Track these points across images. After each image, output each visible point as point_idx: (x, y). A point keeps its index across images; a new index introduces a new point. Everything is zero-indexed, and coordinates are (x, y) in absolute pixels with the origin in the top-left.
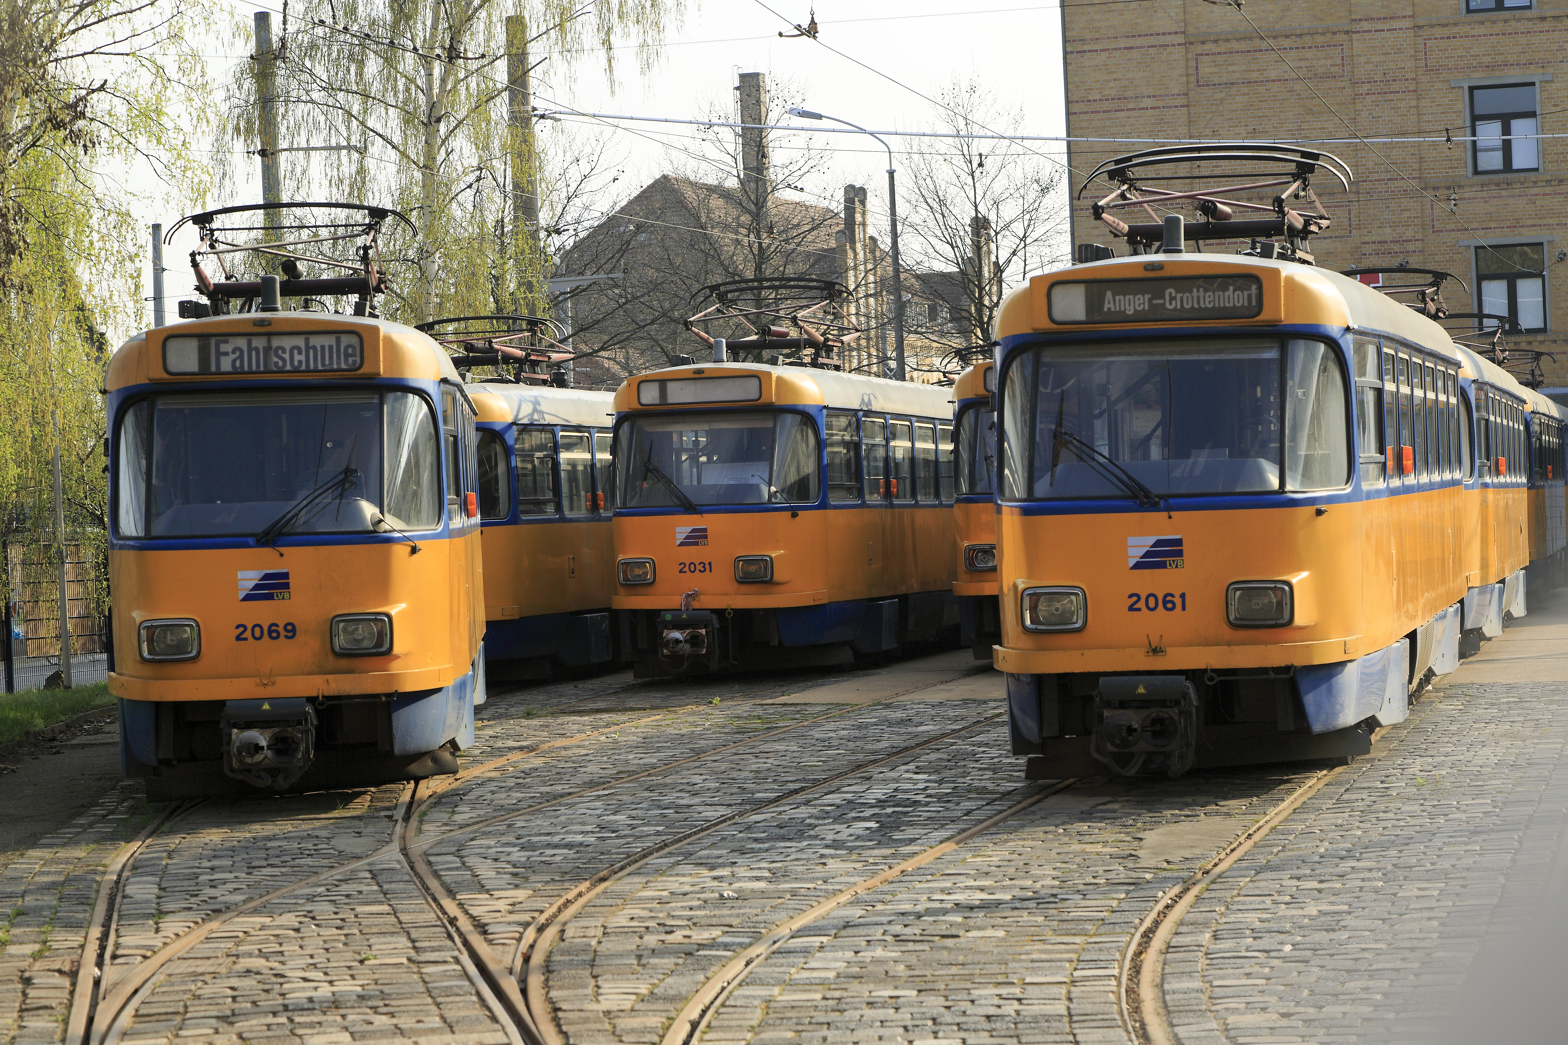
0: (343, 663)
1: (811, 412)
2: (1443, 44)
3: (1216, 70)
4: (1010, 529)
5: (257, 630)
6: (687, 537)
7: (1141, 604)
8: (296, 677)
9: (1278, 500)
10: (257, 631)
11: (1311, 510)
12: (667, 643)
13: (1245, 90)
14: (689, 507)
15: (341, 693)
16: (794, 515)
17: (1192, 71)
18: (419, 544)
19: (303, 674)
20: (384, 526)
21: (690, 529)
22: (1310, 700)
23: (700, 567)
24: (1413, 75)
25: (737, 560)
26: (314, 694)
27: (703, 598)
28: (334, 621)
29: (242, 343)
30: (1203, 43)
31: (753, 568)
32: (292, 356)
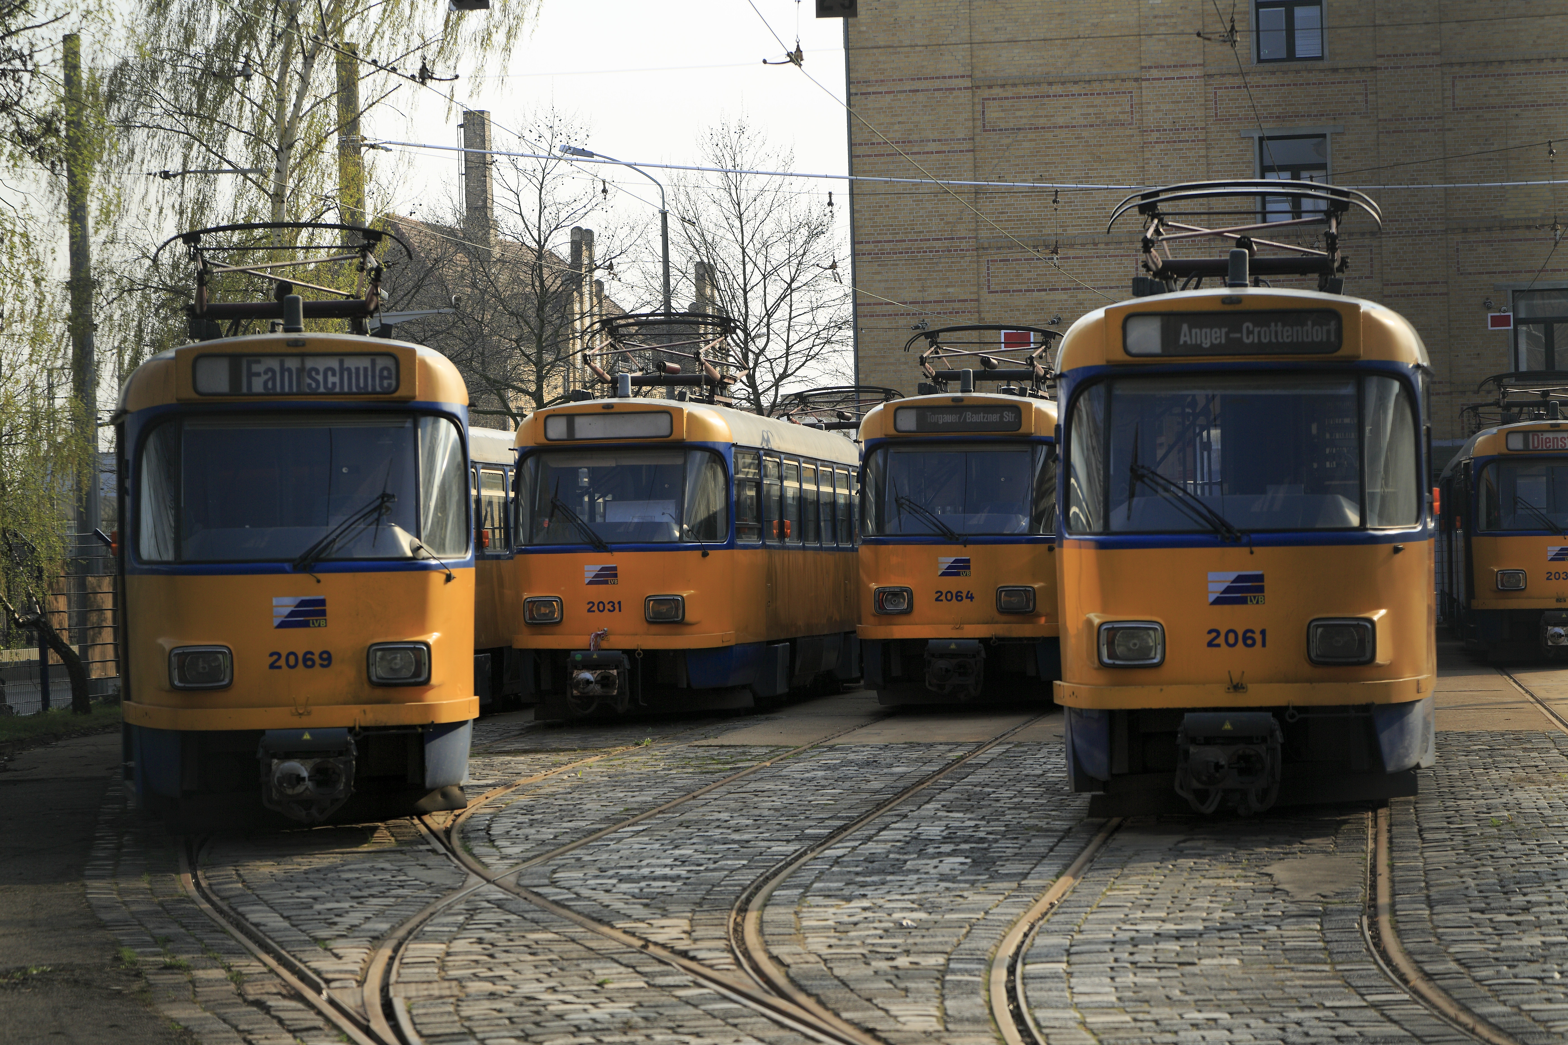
0: (379, 693)
1: (721, 449)
3: (1002, 115)
4: (1076, 562)
6: (596, 576)
7: (1221, 640)
8: (333, 707)
9: (1359, 538)
10: (292, 659)
11: (1388, 547)
12: (577, 684)
13: (1031, 135)
14: (599, 546)
15: (379, 724)
16: (705, 555)
17: (978, 115)
18: (454, 572)
19: (337, 703)
20: (423, 553)
21: (599, 567)
22: (1385, 738)
23: (609, 607)
24: (1203, 125)
25: (647, 599)
26: (351, 725)
27: (612, 638)
28: (370, 651)
29: (275, 364)
30: (990, 87)
31: (664, 608)
32: (328, 379)
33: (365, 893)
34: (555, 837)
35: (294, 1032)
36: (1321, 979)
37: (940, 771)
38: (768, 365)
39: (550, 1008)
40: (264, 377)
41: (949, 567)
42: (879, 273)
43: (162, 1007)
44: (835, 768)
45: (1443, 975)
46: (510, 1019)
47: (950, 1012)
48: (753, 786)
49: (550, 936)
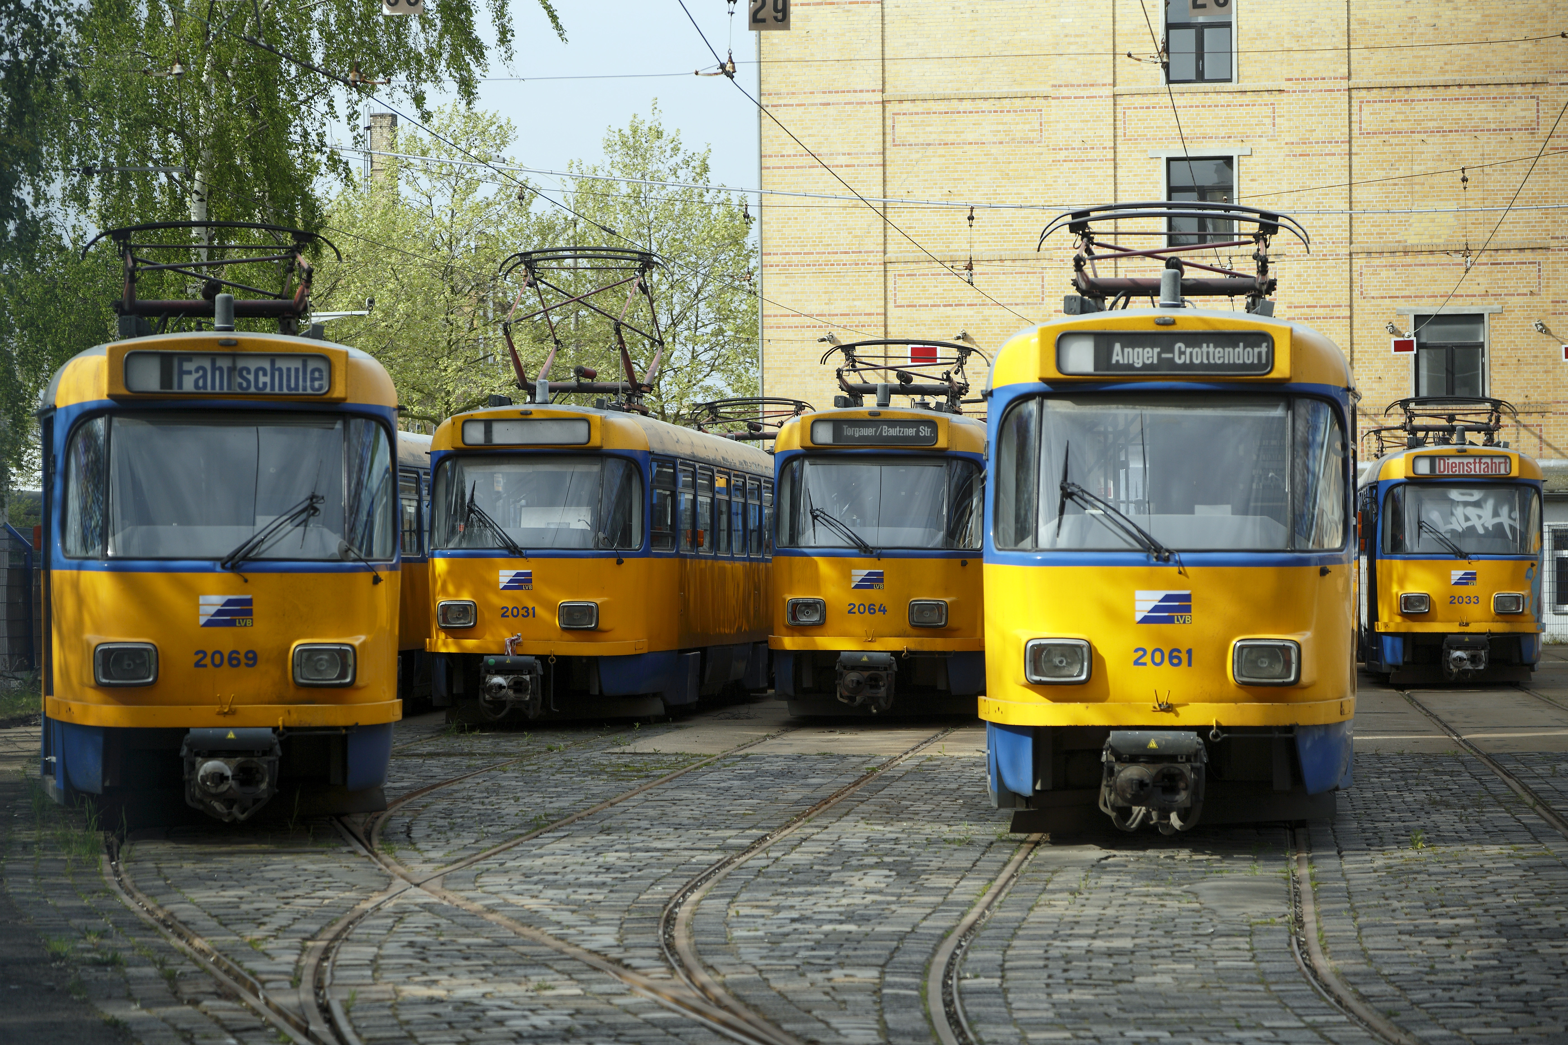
2: (1142, 113)
3: (913, 130)
5: (217, 657)
7: (1147, 659)
10: (217, 657)
13: (941, 150)
15: (303, 724)
16: (620, 562)
30: (901, 101)
33: (291, 893)
34: (477, 841)
35: (233, 1032)
36: (1257, 999)
37: (856, 783)
38: (672, 373)
39: (490, 1014)
40: (195, 376)
41: (863, 580)
42: (786, 285)
43: (99, 1005)
44: (750, 778)
45: (1379, 998)
46: (450, 1023)
47: (890, 1026)
48: (670, 794)
49: (482, 941)
